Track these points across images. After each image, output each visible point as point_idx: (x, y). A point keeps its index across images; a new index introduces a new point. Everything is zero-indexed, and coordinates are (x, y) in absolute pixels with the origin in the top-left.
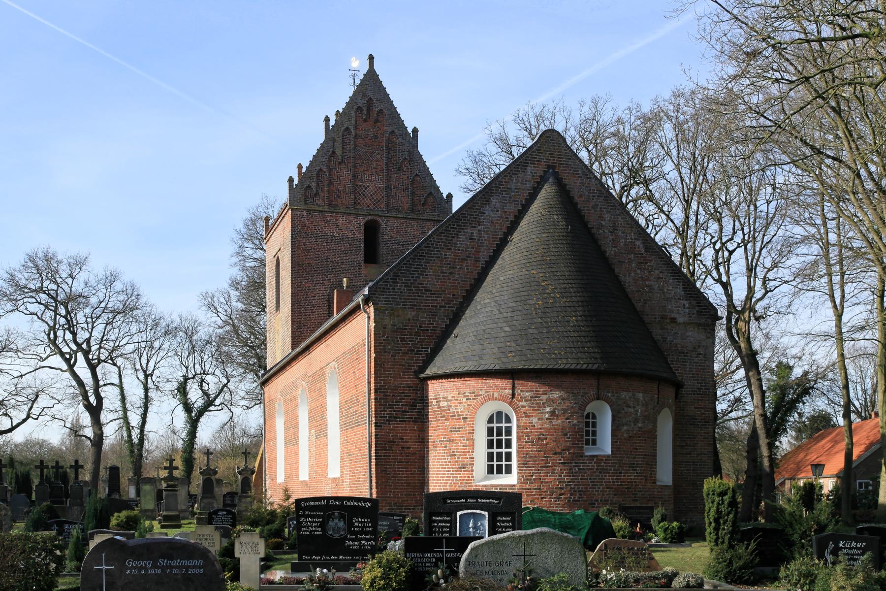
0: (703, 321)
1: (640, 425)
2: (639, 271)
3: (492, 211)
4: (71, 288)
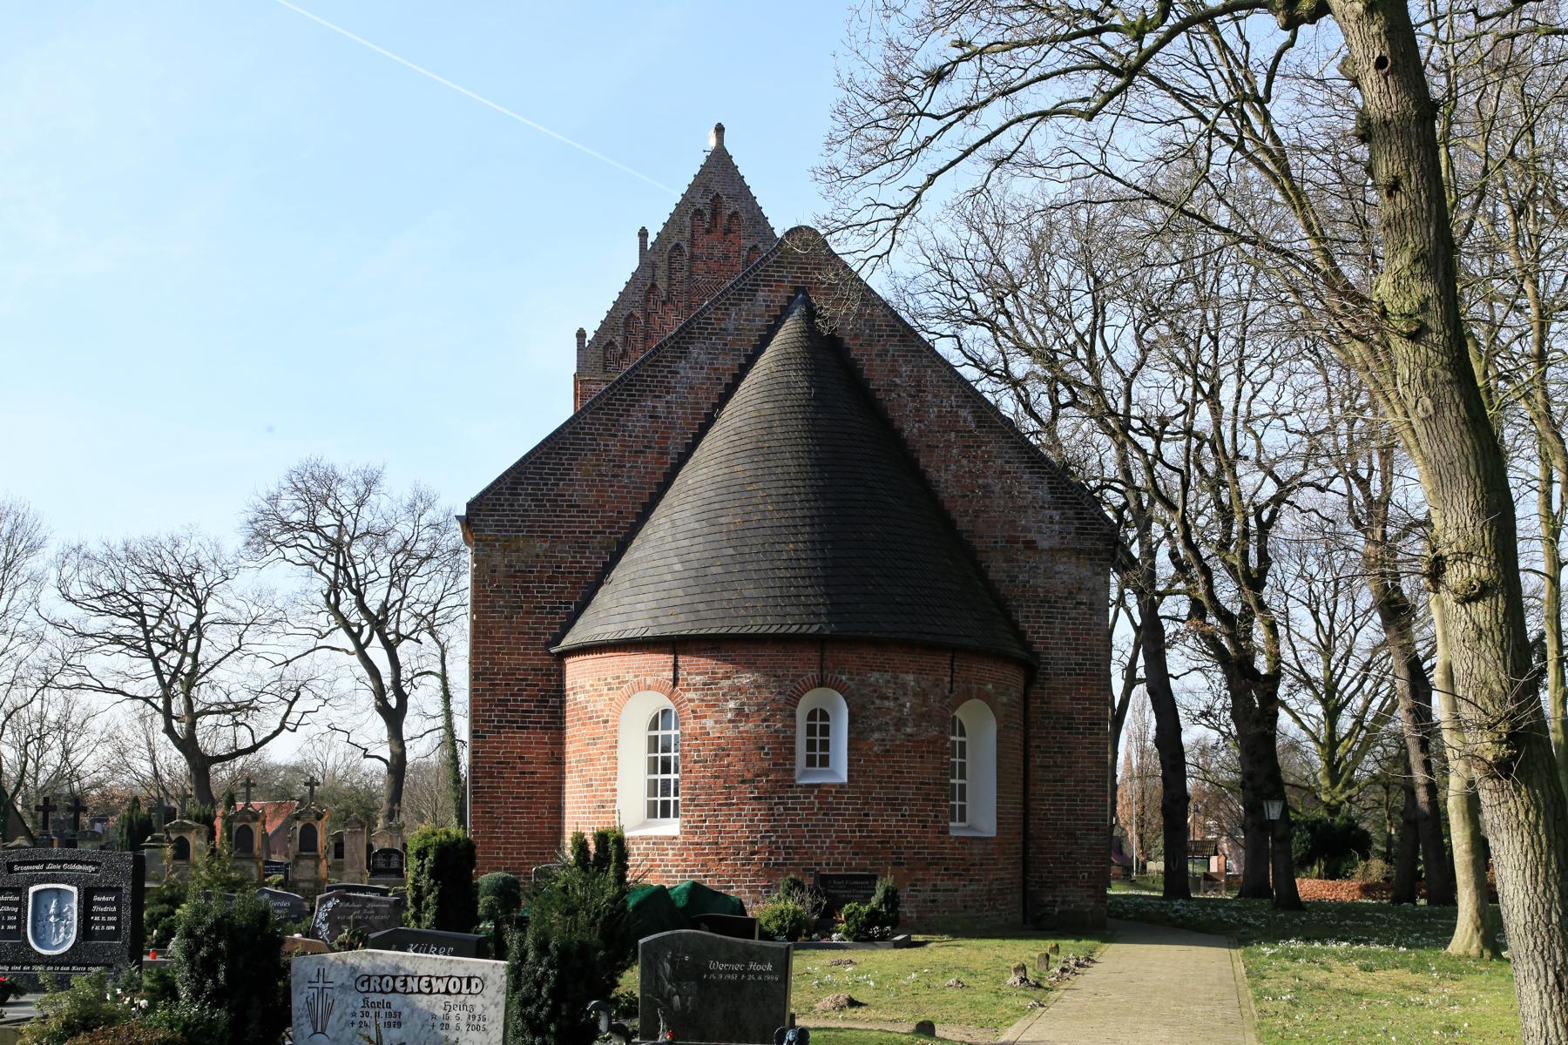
0: (1087, 544)
1: (909, 730)
2: (964, 462)
3: (691, 368)
4: (356, 521)
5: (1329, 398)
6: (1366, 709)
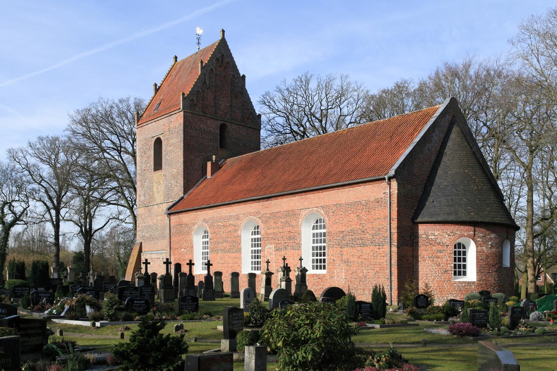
5: (496, 162)
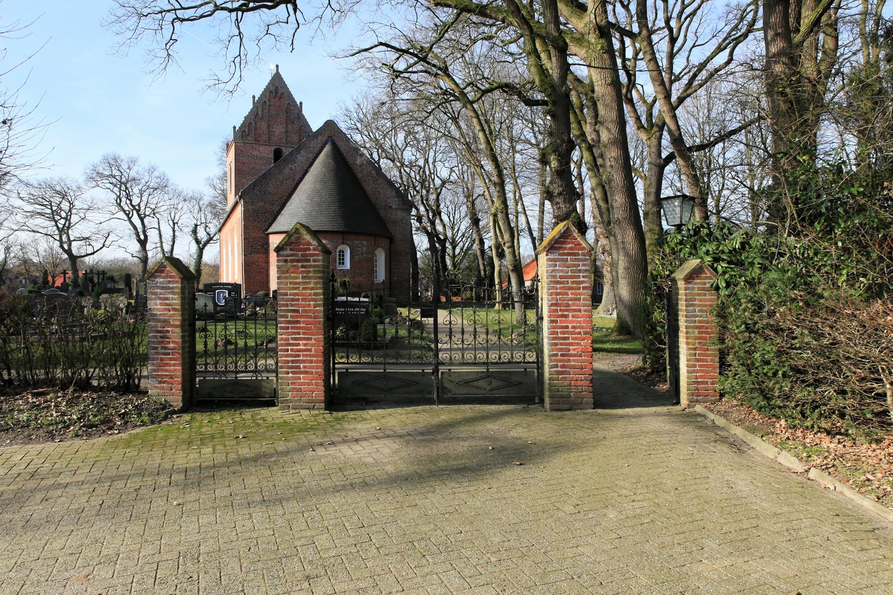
6: (464, 246)
